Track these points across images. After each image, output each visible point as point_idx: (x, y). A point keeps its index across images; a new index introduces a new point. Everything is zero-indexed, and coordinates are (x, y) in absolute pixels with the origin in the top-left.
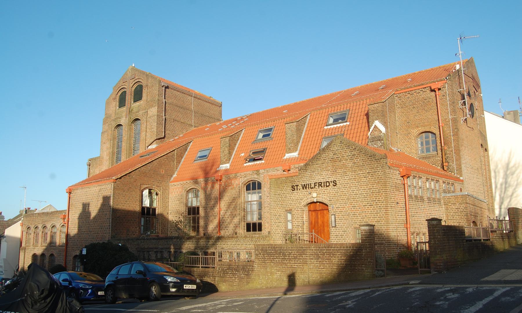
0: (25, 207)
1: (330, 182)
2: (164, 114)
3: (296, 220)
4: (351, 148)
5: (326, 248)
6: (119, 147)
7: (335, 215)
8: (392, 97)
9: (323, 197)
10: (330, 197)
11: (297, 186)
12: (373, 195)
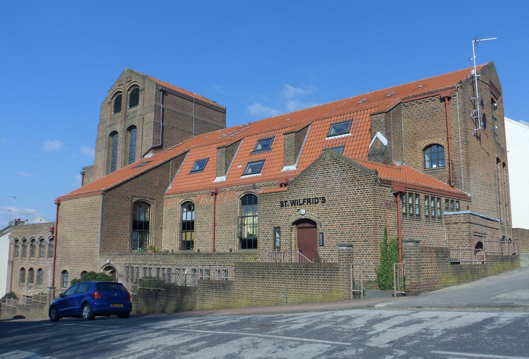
0: (14, 218)
1: (319, 199)
2: (161, 121)
3: (284, 237)
6: (114, 156)
7: (323, 233)
8: (399, 106)
10: (319, 214)
11: (286, 202)
12: (362, 213)
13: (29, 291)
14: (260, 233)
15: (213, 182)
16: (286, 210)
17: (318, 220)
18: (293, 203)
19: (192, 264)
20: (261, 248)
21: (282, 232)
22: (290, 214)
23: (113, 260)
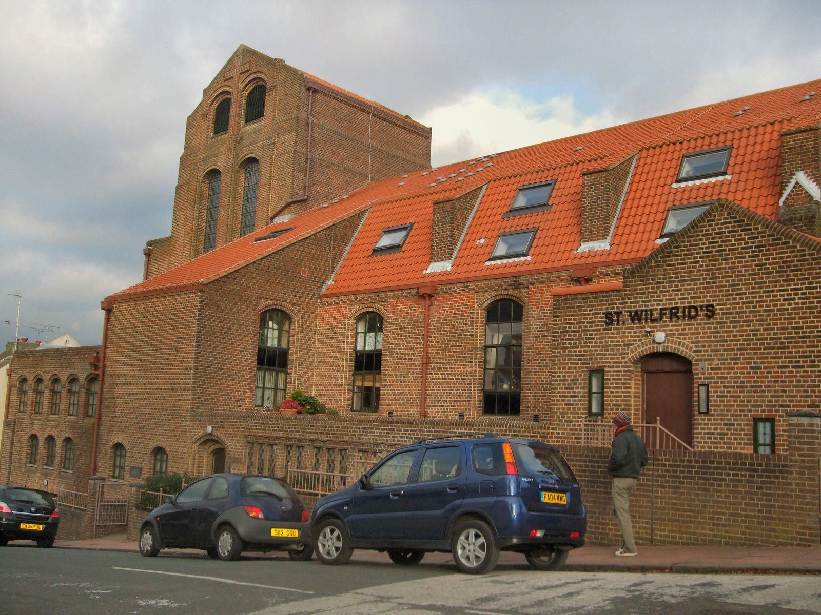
1: (699, 309)
4: (753, 231)
5: (699, 463)
7: (707, 386)
9: (680, 342)
11: (618, 314)
12: (805, 342)
13: (46, 482)
14: (556, 381)
15: (424, 272)
16: (618, 333)
17: (698, 356)
18: (636, 317)
19: (396, 442)
20: (556, 413)
21: (609, 380)
22: (629, 341)
23: (219, 427)
